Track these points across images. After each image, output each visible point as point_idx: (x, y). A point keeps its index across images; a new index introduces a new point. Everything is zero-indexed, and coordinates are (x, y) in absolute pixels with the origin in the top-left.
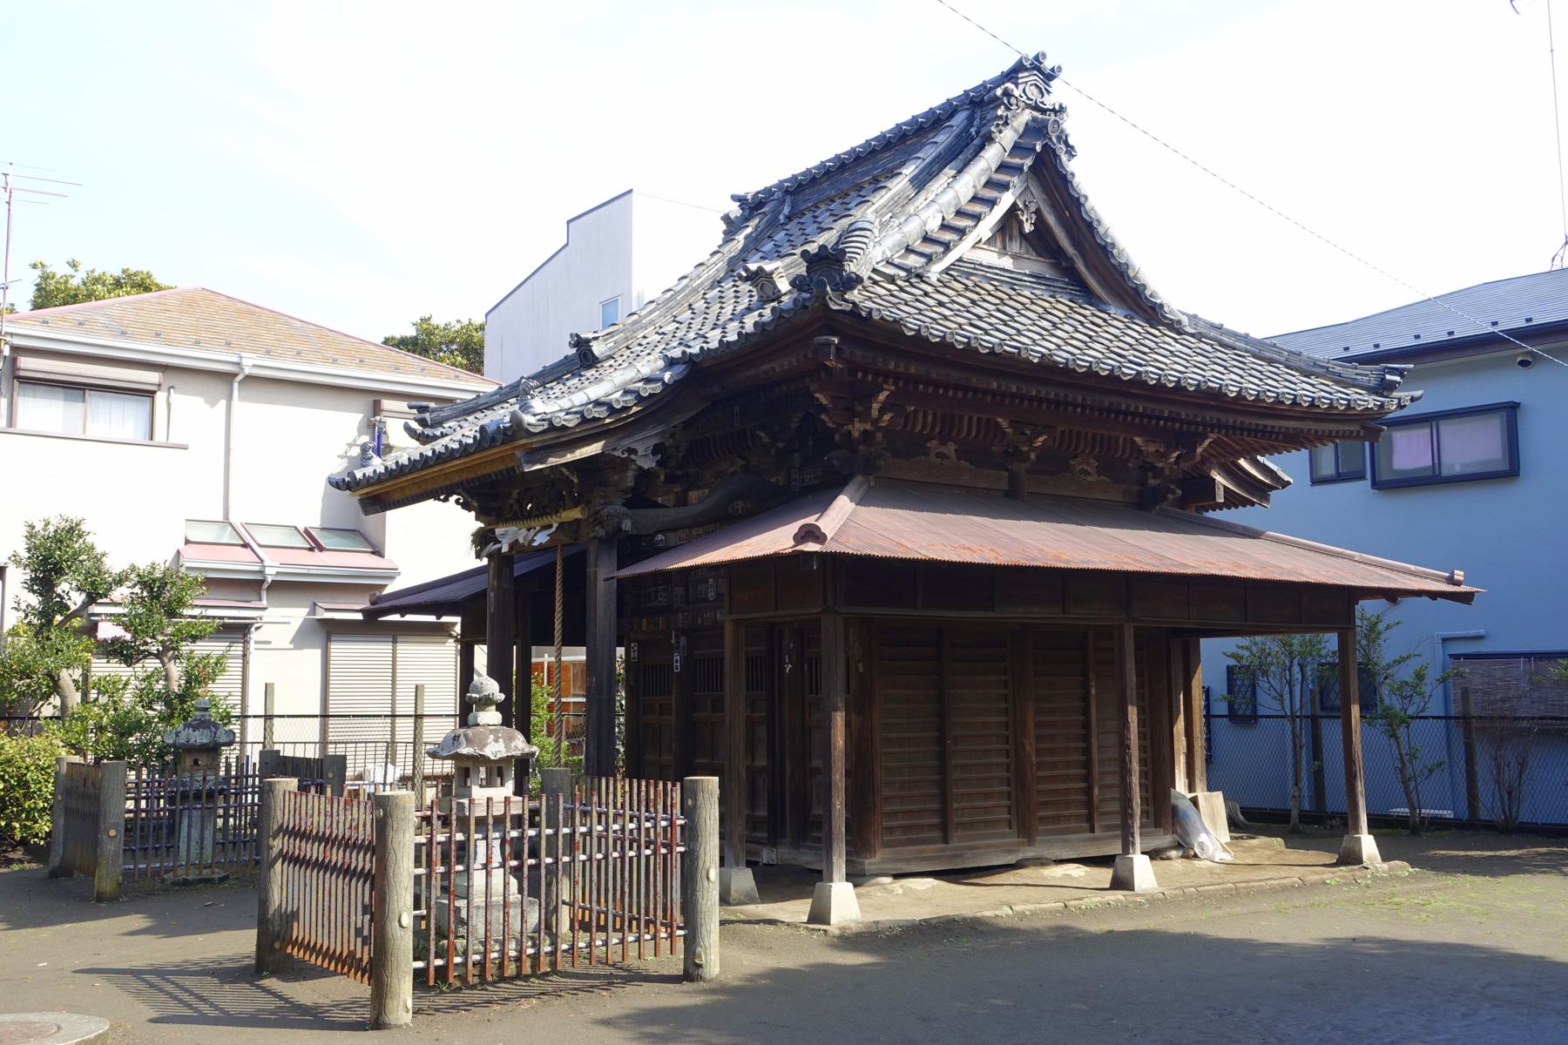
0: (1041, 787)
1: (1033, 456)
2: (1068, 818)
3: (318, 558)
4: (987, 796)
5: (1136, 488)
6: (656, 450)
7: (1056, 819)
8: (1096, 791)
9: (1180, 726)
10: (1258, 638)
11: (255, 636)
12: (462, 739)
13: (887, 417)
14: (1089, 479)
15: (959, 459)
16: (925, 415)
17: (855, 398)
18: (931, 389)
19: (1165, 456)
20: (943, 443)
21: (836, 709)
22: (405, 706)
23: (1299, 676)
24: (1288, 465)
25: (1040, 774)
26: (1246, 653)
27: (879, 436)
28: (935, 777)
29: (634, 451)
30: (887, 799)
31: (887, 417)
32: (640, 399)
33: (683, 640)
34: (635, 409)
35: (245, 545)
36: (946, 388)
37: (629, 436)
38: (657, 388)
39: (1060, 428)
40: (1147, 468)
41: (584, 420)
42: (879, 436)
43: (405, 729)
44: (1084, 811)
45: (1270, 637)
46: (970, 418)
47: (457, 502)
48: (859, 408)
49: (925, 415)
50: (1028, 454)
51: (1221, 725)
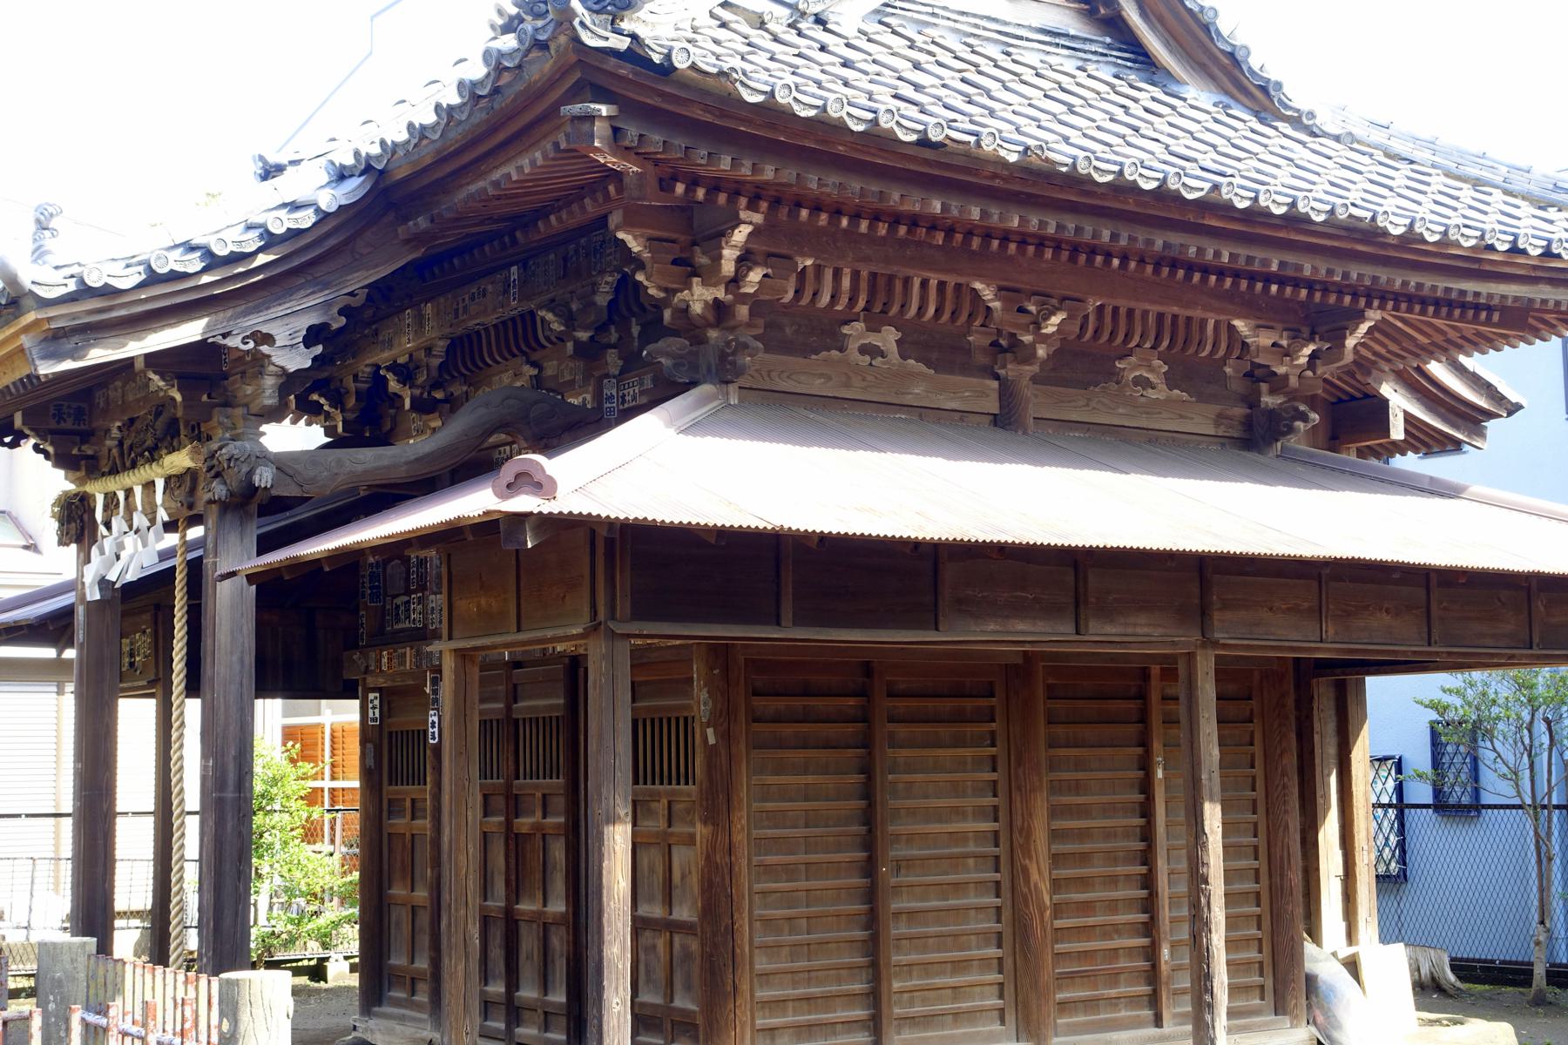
0: (1059, 947)
1: (1041, 352)
2: (1113, 1002)
4: (959, 966)
5: (1239, 411)
6: (313, 335)
7: (1090, 1004)
8: (1165, 952)
9: (1329, 833)
10: (1477, 675)
13: (755, 276)
14: (1152, 394)
15: (904, 357)
16: (837, 274)
17: (691, 242)
18: (823, 218)
19: (1288, 353)
20: (874, 328)
21: (613, 819)
23: (1546, 739)
24: (1521, 369)
25: (1058, 923)
26: (1458, 702)
27: (743, 311)
28: (860, 934)
29: (268, 339)
30: (765, 976)
31: (755, 276)
32: (270, 240)
34: (262, 259)
36: (856, 217)
37: (256, 310)
38: (306, 219)
39: (1093, 304)
40: (1258, 375)
41: (153, 279)
42: (743, 311)
44: (1146, 989)
45: (1496, 673)
46: (924, 284)
47: (36, 448)
48: (702, 260)
49: (837, 274)
50: (1032, 347)
51: (1423, 823)
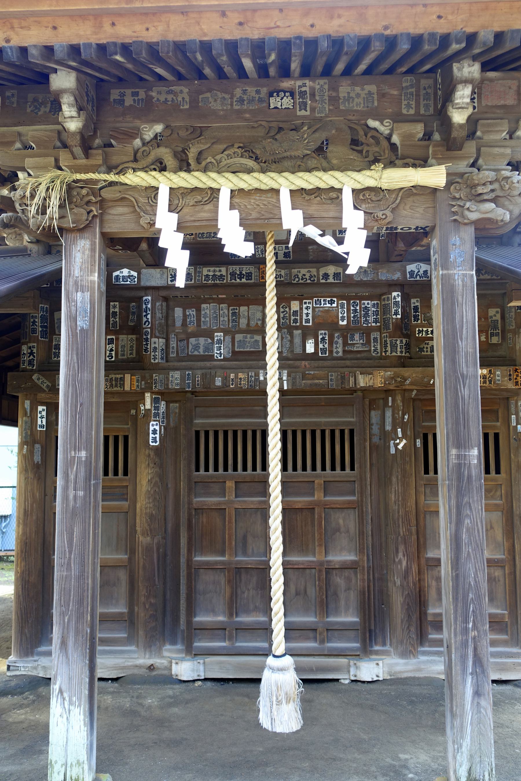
33: (163, 405)
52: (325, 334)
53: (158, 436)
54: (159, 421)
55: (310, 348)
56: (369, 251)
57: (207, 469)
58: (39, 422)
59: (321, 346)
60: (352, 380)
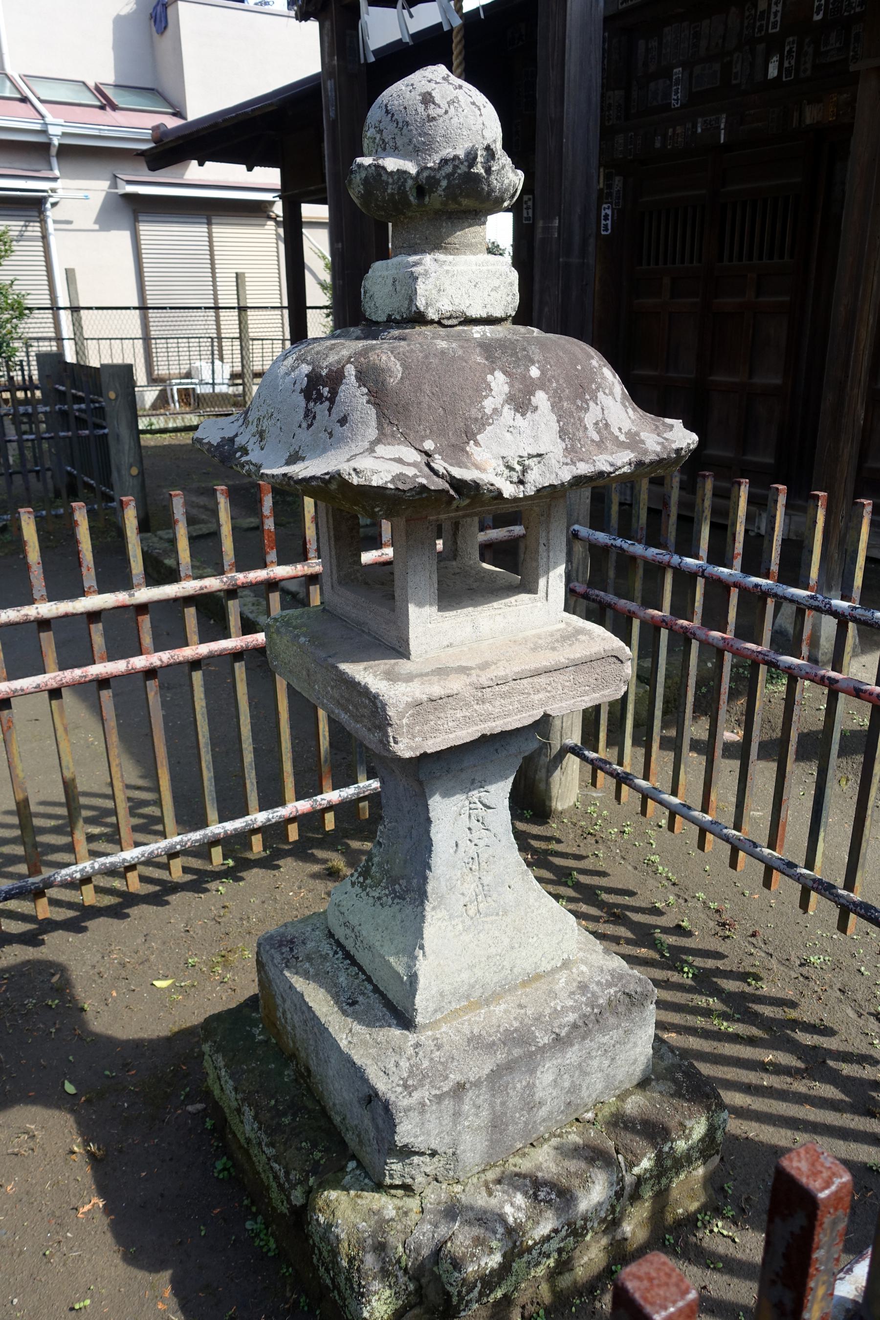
3: (110, 116)
11: (51, 214)
12: (353, 393)
22: (228, 298)
33: (618, 182)
35: (24, 100)
43: (230, 322)
52: (793, 42)
53: (609, 222)
54: (611, 203)
55: (773, 71)
56: (313, 26)
57: (657, 264)
58: (525, 215)
59: (786, 64)
60: (796, 115)
